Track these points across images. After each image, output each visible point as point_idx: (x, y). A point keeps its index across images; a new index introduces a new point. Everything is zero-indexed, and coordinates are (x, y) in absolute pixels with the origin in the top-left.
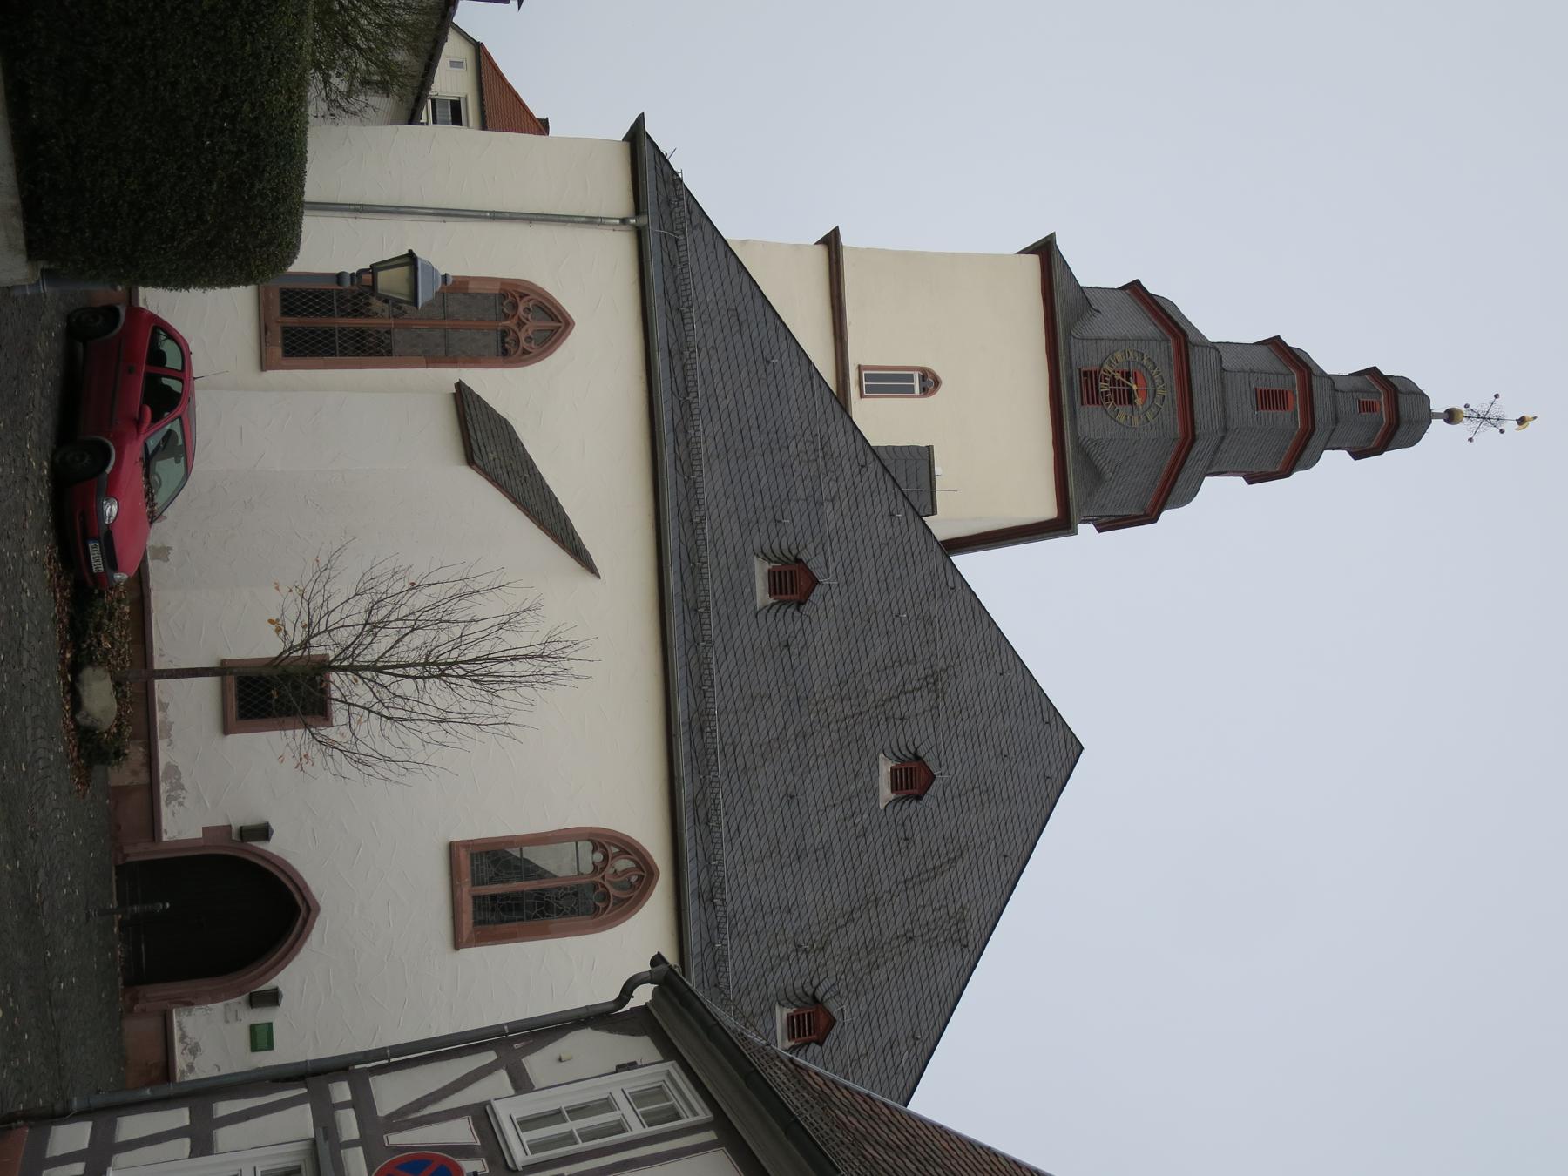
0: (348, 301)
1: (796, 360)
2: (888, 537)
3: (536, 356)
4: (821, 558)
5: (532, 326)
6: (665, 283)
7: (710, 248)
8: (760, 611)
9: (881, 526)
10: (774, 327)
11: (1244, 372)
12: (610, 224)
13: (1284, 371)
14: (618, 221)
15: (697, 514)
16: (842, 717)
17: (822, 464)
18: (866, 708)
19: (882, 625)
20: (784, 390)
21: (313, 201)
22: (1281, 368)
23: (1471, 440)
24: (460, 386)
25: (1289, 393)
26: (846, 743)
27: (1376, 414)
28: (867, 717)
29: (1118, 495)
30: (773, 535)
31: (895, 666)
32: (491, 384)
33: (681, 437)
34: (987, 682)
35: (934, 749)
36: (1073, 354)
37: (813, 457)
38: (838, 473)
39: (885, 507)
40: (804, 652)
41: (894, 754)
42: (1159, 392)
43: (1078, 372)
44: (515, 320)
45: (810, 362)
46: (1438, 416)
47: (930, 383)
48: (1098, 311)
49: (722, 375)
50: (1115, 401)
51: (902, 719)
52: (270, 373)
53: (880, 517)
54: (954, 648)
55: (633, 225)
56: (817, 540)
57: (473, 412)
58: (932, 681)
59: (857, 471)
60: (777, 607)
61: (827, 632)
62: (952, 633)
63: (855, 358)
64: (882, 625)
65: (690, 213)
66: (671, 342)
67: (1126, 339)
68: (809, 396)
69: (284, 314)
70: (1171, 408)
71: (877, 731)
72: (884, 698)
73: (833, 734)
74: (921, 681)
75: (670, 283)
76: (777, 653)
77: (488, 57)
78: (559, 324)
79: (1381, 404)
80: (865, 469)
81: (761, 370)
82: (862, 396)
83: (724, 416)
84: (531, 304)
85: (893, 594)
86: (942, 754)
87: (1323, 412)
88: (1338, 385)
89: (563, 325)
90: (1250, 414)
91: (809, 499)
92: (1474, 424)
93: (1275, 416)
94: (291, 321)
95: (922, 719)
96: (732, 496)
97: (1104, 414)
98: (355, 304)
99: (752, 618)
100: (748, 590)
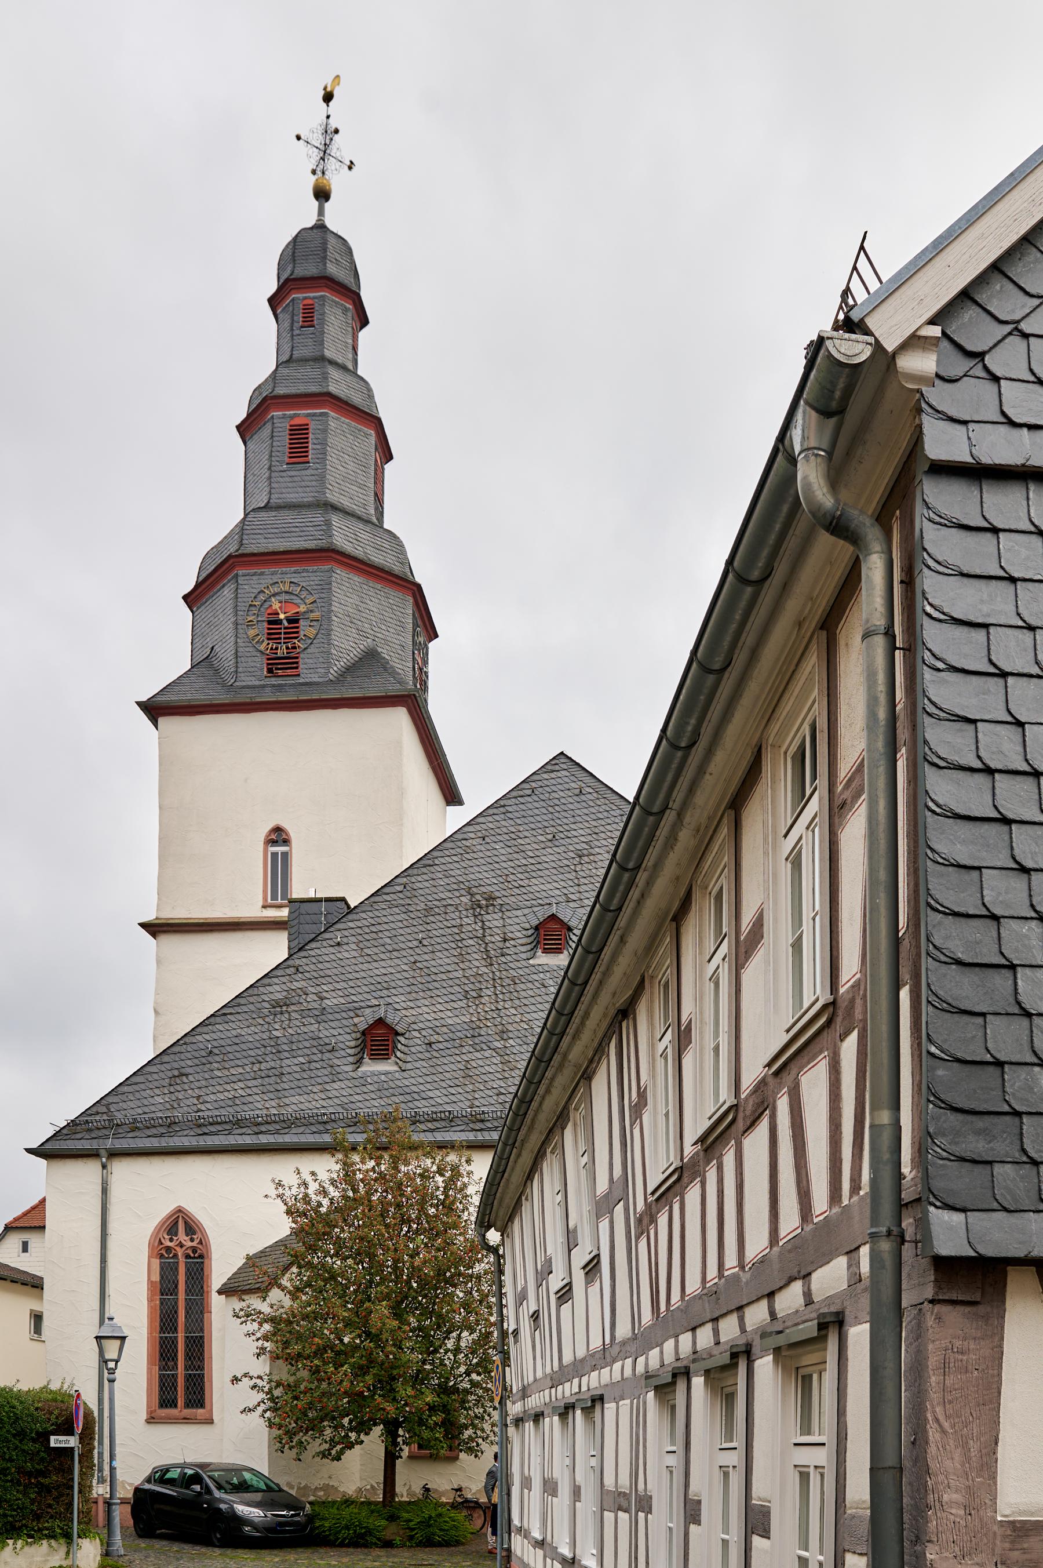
0: (166, 1364)
1: (210, 1027)
2: (356, 948)
3: (202, 1234)
4: (368, 1011)
5: (182, 1237)
6: (149, 1136)
7: (124, 1097)
8: (400, 1068)
9: (346, 955)
10: (185, 1046)
11: (270, 478)
12: (107, 1177)
13: (269, 426)
14: (105, 1171)
15: (320, 1118)
17: (293, 1008)
18: (491, 975)
19: (426, 957)
20: (233, 1039)
21: (836, 1376)
22: (266, 431)
24: (220, 1292)
25: (293, 423)
26: (515, 994)
27: (316, 305)
28: (497, 973)
29: (392, 630)
30: (343, 1053)
31: (461, 945)
32: (221, 1270)
33: (263, 1128)
34: (488, 853)
35: (535, 909)
36: (250, 683)
37: (287, 1015)
38: (301, 993)
39: (332, 950)
40: (437, 1030)
41: (532, 949)
42: (287, 589)
43: (268, 679)
44: (178, 1249)
45: (212, 1015)
46: (321, 212)
47: (278, 836)
48: (212, 648)
49: (219, 1092)
50: (296, 638)
51: (505, 940)
53: (339, 955)
54: (455, 887)
56: (352, 1014)
57: (236, 1285)
58: (478, 910)
59: (300, 975)
61: (425, 1009)
62: (441, 889)
63: (254, 911)
64: (426, 957)
65: (98, 1113)
66: (192, 1133)
67: (236, 624)
68: (239, 1017)
69: (176, 1406)
70: (303, 575)
71: (511, 965)
72: (485, 957)
73: (507, 1006)
74: (477, 921)
75: (149, 1132)
76: (435, 1054)
77: (16, 1220)
78: (180, 1218)
79: (305, 298)
80: (300, 968)
81: (217, 1058)
83: (249, 1091)
84: (166, 1237)
85: (403, 946)
86: (540, 902)
88: (285, 358)
89: (181, 1215)
90: (313, 472)
91: (320, 1020)
92: (331, 164)
94: (180, 1402)
95: (508, 920)
96: (310, 1088)
97: (309, 651)
98: (168, 1359)
99: (405, 1074)
100: (383, 1077)
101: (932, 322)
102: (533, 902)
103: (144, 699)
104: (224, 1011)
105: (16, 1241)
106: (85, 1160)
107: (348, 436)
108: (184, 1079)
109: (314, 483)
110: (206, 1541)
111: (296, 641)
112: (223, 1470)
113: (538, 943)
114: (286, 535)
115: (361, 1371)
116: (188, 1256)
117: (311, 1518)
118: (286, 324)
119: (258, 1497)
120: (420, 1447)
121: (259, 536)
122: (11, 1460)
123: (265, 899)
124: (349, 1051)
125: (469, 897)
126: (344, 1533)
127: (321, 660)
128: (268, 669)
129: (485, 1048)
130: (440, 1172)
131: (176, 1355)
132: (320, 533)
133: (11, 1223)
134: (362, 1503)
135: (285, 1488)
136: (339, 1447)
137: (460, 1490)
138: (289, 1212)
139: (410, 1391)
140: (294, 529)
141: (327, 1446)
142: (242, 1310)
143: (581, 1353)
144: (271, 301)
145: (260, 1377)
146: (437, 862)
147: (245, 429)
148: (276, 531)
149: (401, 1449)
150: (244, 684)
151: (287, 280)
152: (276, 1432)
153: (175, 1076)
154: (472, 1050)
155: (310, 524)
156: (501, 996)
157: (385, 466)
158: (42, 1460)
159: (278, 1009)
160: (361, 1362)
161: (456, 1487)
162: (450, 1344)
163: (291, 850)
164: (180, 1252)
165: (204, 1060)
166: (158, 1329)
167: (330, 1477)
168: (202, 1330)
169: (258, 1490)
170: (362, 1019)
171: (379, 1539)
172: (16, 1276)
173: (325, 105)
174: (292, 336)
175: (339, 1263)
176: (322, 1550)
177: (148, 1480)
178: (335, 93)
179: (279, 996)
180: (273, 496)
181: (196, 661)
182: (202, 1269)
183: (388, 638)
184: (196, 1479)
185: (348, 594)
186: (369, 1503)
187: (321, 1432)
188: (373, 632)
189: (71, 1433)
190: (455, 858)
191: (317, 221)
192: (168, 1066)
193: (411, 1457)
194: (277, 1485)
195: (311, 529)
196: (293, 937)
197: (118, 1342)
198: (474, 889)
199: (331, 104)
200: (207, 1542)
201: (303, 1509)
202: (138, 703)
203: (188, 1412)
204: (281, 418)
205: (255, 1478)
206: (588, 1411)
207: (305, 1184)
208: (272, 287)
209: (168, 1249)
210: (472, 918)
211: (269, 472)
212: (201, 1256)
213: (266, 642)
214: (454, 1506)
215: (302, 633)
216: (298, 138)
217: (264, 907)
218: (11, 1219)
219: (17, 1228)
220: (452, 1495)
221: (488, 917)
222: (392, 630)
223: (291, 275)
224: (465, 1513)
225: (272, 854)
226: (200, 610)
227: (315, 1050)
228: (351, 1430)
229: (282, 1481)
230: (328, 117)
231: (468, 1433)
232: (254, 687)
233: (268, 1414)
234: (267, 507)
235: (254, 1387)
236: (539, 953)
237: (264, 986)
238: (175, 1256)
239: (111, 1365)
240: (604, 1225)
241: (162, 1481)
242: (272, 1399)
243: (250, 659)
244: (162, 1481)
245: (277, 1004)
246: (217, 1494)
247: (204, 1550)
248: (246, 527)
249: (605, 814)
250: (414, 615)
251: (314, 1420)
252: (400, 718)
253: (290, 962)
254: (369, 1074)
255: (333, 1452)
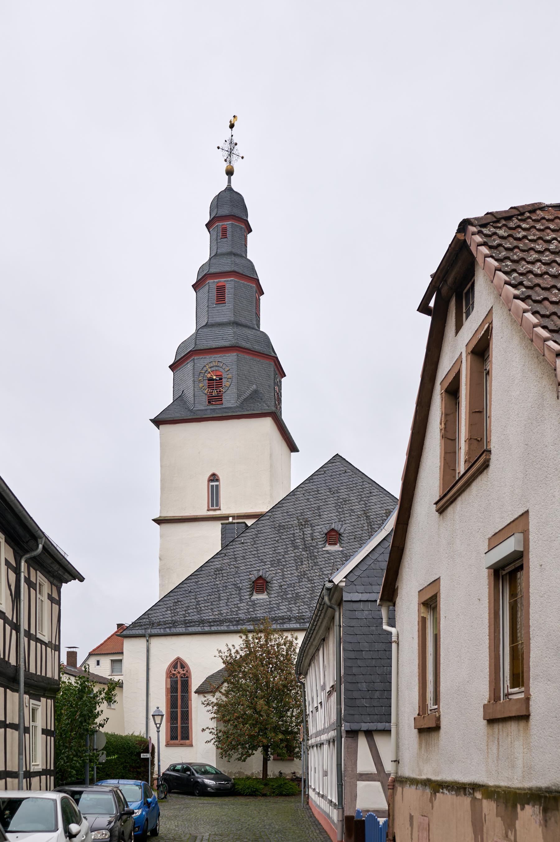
4: (255, 572)
5: (179, 669)
7: (155, 611)
11: (208, 311)
13: (207, 287)
16: (308, 565)
22: (206, 288)
23: (242, 158)
24: (196, 692)
25: (218, 285)
27: (228, 228)
32: (196, 683)
37: (221, 575)
42: (216, 365)
44: (178, 674)
46: (229, 181)
47: (214, 478)
48: (183, 391)
50: (221, 387)
52: (193, 744)
55: (149, 638)
56: (248, 574)
60: (268, 590)
63: (203, 512)
66: (183, 626)
67: (194, 381)
69: (177, 739)
70: (224, 358)
77: (94, 650)
78: (179, 662)
79: (223, 225)
81: (193, 594)
82: (220, 509)
84: (173, 669)
87: (226, 265)
89: (179, 660)
90: (228, 307)
92: (234, 157)
93: (228, 293)
94: (179, 738)
101: (344, 578)
102: (325, 522)
103: (153, 418)
104: (195, 574)
105: (94, 660)
106: (139, 638)
107: (243, 289)
108: (179, 603)
109: (228, 313)
110: (192, 794)
111: (221, 388)
112: (198, 766)
113: (326, 541)
114: (216, 339)
115: (254, 725)
116: (182, 677)
117: (234, 785)
118: (215, 237)
119: (212, 776)
120: (278, 756)
121: (204, 340)
122: (128, 763)
123: (208, 507)
124: (248, 590)
125: (297, 521)
126: (247, 791)
127: (232, 396)
128: (208, 401)
129: (304, 587)
130: (285, 644)
131: (177, 718)
132: (231, 338)
133: (92, 652)
134: (254, 779)
135: (223, 773)
136: (245, 756)
137: (294, 773)
138: (224, 662)
139: (273, 734)
140: (219, 337)
141: (240, 756)
142: (205, 701)
143: (320, 729)
144: (207, 225)
145: (213, 729)
146: (284, 505)
147: (196, 287)
148: (211, 337)
149: (270, 757)
150: (198, 409)
151: (214, 217)
152: (220, 751)
153: (176, 602)
154: (298, 588)
155: (227, 334)
156: (311, 564)
157: (261, 330)
158: (138, 763)
159: (218, 572)
160: (253, 722)
161: (293, 772)
162: (289, 714)
163: (220, 484)
164: (179, 676)
165: (187, 595)
166: (170, 707)
167: (241, 768)
168: (188, 708)
169: (212, 774)
170: (253, 576)
171: (261, 793)
172: (101, 681)
173: (230, 129)
174: (217, 243)
175: (244, 681)
176: (238, 797)
177: (168, 770)
178: (235, 124)
179: (218, 566)
180: (209, 319)
181: (175, 398)
182: (188, 683)
183: (263, 383)
184: (188, 769)
185: (244, 365)
186: (257, 779)
187: (238, 750)
188: (255, 381)
189: (148, 752)
190: (291, 504)
191: (228, 186)
192: (173, 598)
193: (274, 760)
194: (220, 771)
195: (227, 336)
196: (223, 539)
197: (160, 717)
198: (300, 517)
199: (233, 129)
200: (193, 794)
201: (231, 781)
202: (151, 420)
203: (182, 742)
204: (213, 283)
205: (211, 769)
206: (320, 746)
207: (230, 650)
208: (207, 219)
209: (174, 674)
210: (299, 530)
211: (207, 308)
212: (187, 677)
213: (207, 389)
214: (292, 780)
215: (224, 385)
216: (218, 148)
217: (208, 510)
218: (91, 650)
219: (94, 654)
220: (291, 775)
221: (305, 529)
222: (264, 379)
223: (216, 215)
224: (296, 783)
225: (211, 486)
226: (177, 373)
227: (233, 590)
228: (250, 749)
229: (221, 770)
230: (232, 136)
231: (297, 750)
232: (202, 410)
233: (216, 743)
234: (206, 325)
235: (211, 733)
236: (327, 545)
237: (212, 562)
238: (177, 677)
239: (158, 725)
240: (322, 693)
241: (174, 770)
242: (218, 737)
243: (200, 397)
244: (174, 770)
245: (217, 570)
246: (197, 775)
247: (192, 797)
248: (197, 336)
249: (356, 481)
250: (274, 370)
251: (235, 745)
252: (268, 423)
253: (222, 552)
254: (256, 599)
255: (243, 758)
